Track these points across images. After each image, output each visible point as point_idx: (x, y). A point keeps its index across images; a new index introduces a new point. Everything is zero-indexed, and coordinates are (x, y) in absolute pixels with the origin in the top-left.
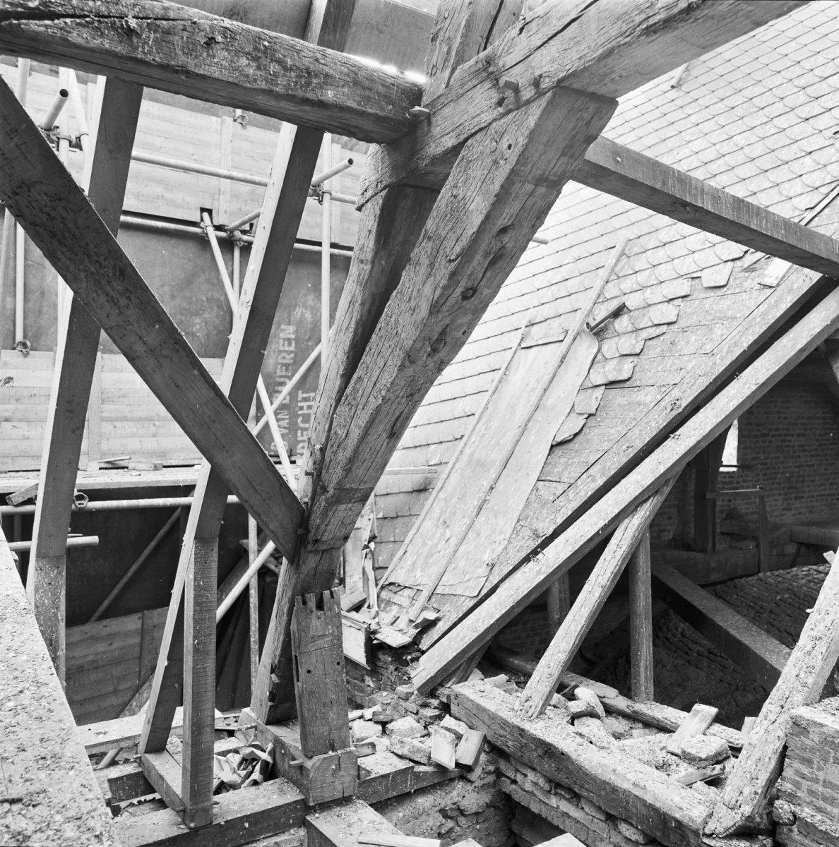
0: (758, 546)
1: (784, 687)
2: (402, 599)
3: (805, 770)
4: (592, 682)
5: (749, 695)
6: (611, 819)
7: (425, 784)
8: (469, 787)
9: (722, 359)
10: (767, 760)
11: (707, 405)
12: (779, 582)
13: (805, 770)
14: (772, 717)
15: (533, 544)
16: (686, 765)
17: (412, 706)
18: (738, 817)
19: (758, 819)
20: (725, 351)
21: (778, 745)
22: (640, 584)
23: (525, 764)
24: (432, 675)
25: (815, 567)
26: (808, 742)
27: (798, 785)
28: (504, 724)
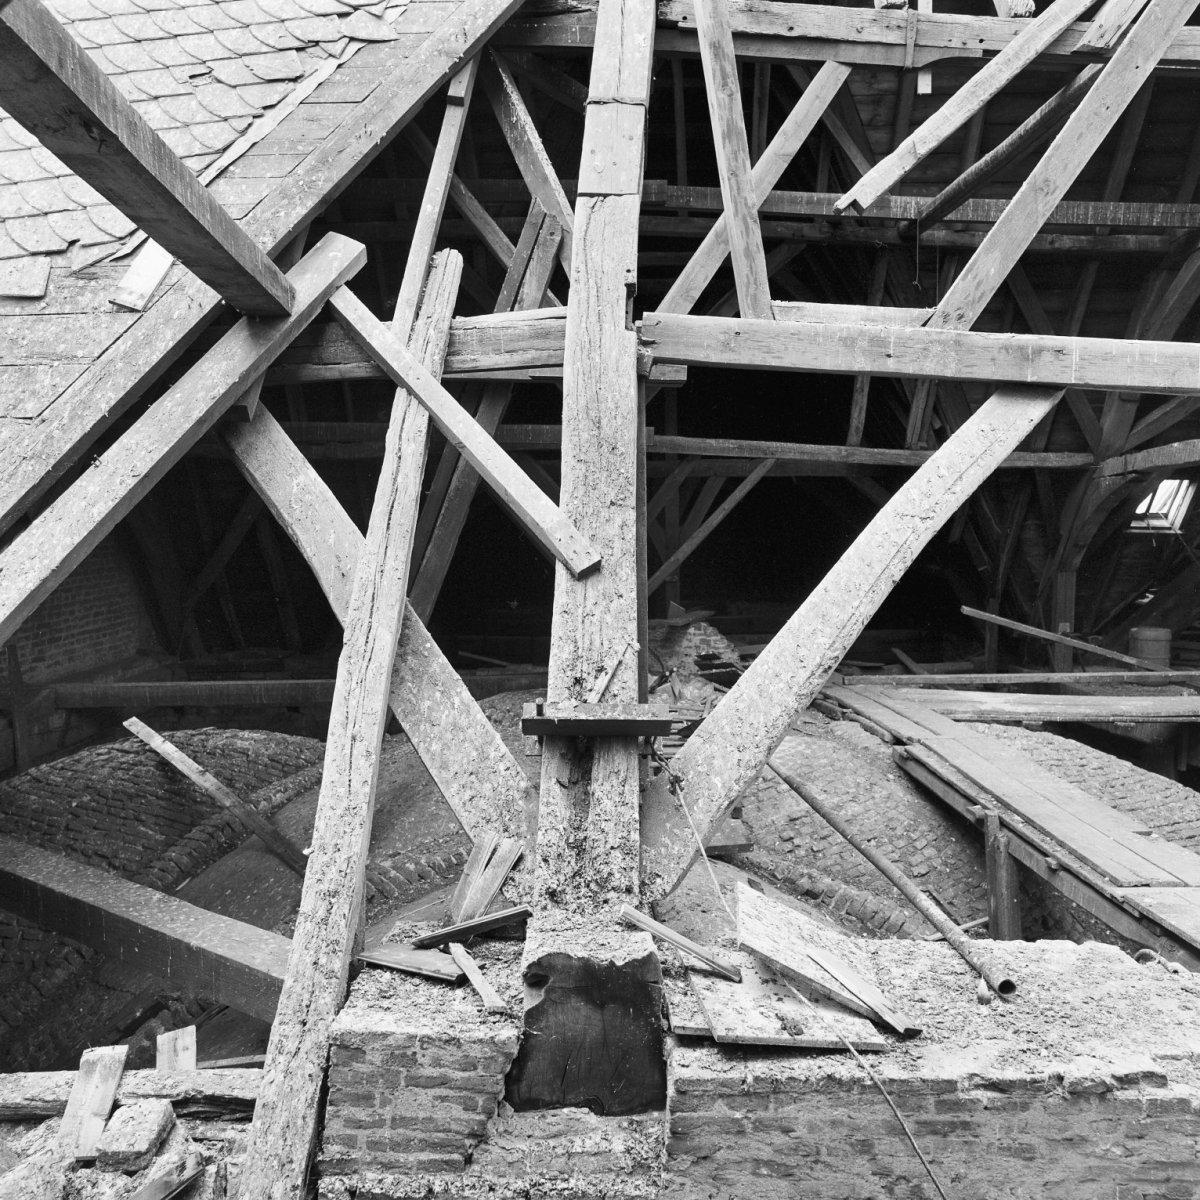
0: (11, 724)
1: (298, 989)
3: (362, 1114)
5: (58, 972)
9: (63, 428)
10: (300, 1122)
11: (46, 513)
12: (70, 779)
13: (362, 1114)
14: (291, 1046)
16: (109, 1176)
20: (66, 415)
25: (117, 746)
27: (350, 1142)
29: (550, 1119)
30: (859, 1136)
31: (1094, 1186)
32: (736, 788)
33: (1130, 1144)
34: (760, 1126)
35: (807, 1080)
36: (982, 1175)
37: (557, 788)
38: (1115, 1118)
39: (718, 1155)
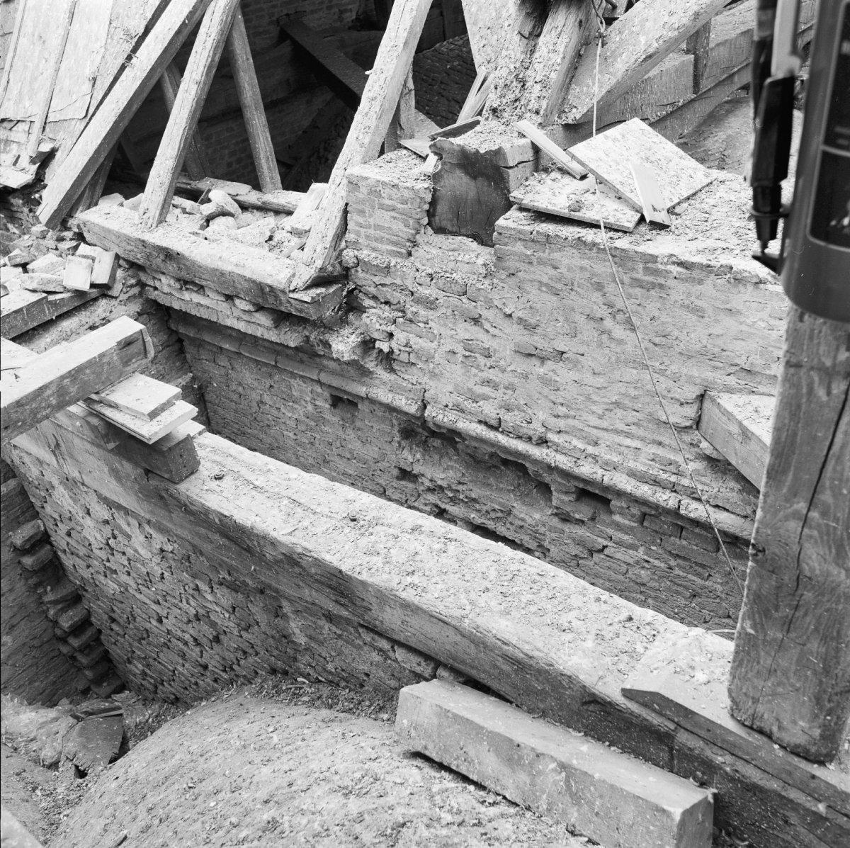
2: (19, 135)
4: (228, 183)
6: (229, 298)
7: (65, 309)
8: (114, 302)
15: (128, 48)
17: (50, 242)
18: (313, 271)
19: (330, 269)
21: (341, 205)
22: (242, 74)
23: (156, 271)
24: (55, 208)
26: (361, 196)
27: (358, 234)
28: (128, 240)
29: (450, 240)
30: (595, 279)
31: (742, 343)
32: (656, 45)
33: (772, 322)
34: (541, 262)
35: (566, 239)
36: (669, 320)
37: (517, 38)
38: (763, 302)
39: (519, 274)
